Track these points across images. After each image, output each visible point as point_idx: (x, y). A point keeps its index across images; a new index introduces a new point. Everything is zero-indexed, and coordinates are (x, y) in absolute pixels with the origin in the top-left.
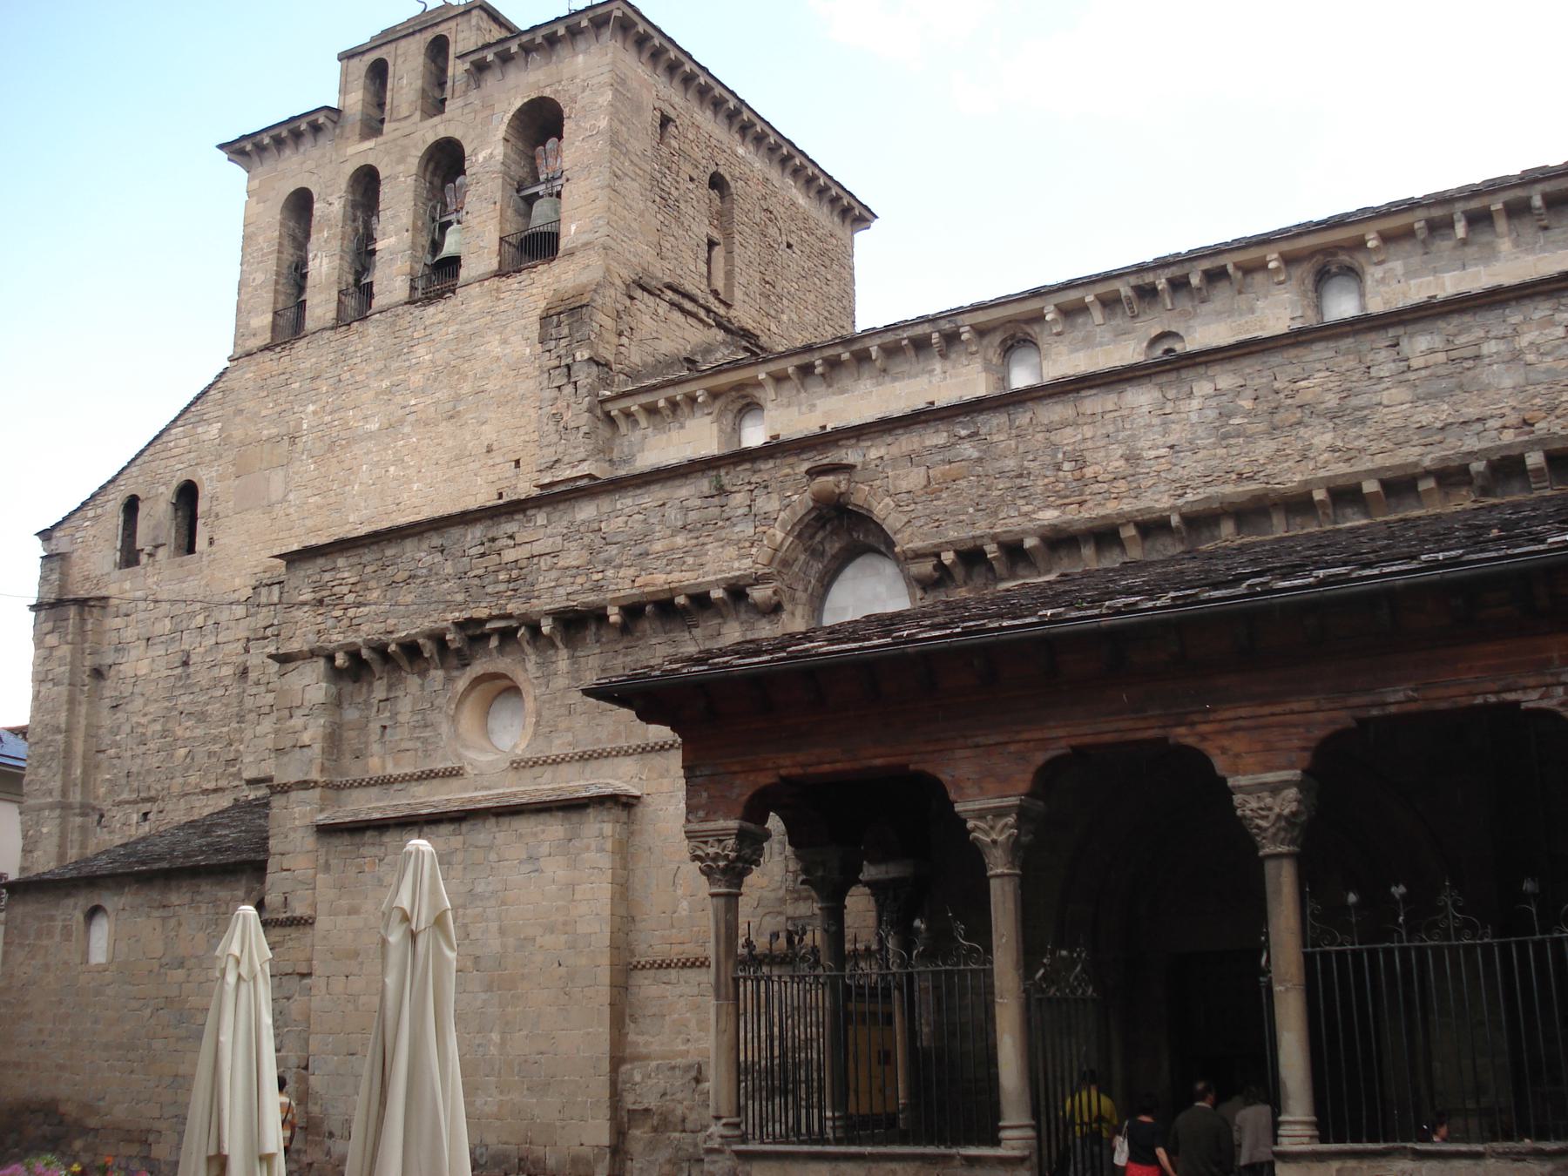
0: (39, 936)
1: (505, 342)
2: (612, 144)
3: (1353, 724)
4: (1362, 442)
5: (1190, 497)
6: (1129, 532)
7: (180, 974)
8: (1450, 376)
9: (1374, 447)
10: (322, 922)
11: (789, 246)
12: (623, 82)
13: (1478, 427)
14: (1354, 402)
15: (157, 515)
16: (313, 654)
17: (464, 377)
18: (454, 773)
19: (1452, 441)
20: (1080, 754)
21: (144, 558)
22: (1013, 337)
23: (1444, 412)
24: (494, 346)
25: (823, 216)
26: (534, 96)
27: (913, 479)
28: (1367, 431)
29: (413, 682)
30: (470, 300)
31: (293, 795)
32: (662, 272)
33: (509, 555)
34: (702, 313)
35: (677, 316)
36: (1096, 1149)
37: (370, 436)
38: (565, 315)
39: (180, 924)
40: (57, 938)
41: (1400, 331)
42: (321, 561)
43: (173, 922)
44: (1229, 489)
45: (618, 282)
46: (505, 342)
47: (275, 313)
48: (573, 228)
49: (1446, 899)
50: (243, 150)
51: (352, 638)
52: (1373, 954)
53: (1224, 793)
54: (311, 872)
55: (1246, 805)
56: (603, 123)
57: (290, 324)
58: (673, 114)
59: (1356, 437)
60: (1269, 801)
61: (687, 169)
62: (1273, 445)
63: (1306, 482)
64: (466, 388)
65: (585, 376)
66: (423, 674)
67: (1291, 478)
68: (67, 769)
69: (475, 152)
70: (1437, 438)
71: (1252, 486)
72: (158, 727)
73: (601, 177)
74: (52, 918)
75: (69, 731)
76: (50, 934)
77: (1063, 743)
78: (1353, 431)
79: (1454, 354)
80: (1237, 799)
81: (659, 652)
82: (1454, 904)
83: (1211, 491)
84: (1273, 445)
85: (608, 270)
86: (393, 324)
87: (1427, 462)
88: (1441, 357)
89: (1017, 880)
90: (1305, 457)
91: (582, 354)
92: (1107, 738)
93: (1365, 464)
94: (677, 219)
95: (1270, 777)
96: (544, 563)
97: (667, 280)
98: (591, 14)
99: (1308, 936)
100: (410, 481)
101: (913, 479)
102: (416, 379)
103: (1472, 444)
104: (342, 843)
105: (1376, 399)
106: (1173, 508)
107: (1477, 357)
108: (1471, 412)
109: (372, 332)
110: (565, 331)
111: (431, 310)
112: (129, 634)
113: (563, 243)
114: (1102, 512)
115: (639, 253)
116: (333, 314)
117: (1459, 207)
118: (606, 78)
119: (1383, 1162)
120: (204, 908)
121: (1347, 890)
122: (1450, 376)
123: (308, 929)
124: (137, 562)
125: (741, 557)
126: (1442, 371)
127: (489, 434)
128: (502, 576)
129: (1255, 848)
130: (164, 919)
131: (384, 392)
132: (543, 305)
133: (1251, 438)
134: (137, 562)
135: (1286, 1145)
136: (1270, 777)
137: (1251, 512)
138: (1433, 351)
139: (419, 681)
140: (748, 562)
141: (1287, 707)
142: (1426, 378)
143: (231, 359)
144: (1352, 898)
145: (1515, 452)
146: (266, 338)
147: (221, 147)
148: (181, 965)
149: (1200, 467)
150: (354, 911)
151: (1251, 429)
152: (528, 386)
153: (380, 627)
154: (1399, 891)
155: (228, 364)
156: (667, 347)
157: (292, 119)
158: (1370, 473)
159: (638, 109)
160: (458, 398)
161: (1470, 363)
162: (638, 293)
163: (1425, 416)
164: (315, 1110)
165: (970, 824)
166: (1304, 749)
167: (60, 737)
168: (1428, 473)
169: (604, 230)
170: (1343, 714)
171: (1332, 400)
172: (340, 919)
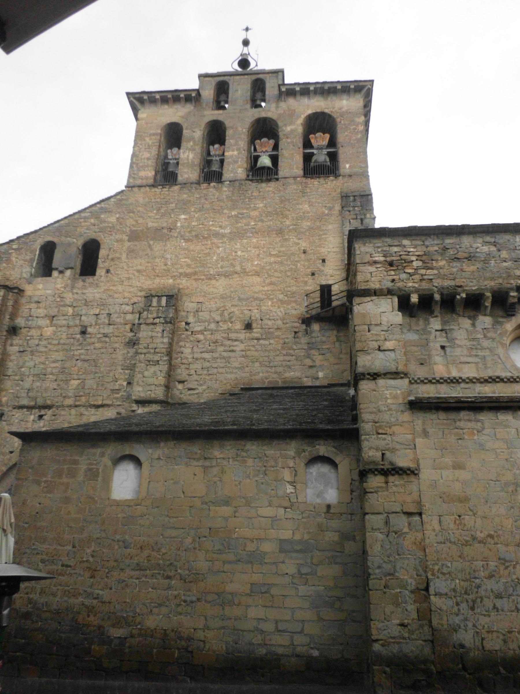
0: (59, 474)
7: (226, 511)
15: (68, 252)
16: (390, 292)
21: (55, 274)
26: (314, 111)
29: (466, 323)
31: (381, 382)
39: (223, 472)
40: (80, 478)
42: (389, 240)
43: (215, 471)
47: (156, 171)
48: (347, 166)
50: (139, 100)
51: (425, 285)
54: (410, 437)
57: (167, 175)
66: (473, 318)
74: (76, 462)
76: (72, 474)
98: (356, 84)
104: (434, 421)
120: (250, 462)
123: (412, 478)
124: (50, 275)
130: (205, 468)
134: (50, 275)
139: (469, 322)
143: (126, 187)
147: (128, 94)
148: (226, 502)
150: (458, 466)
155: (124, 188)
157: (176, 91)
172: (445, 473)
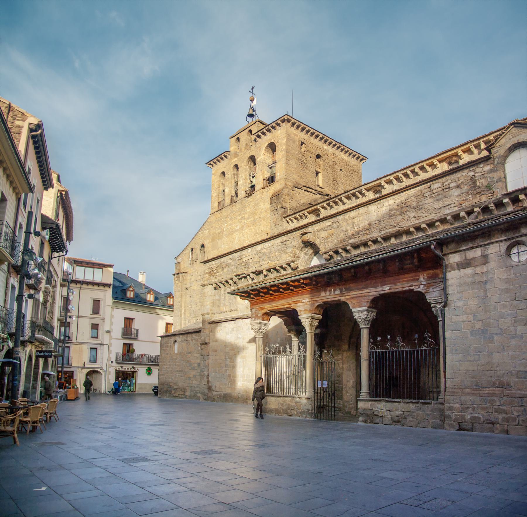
1: (264, 205)
2: (287, 152)
3: (378, 296)
4: (421, 215)
5: (382, 233)
6: (370, 243)
7: (190, 355)
8: (442, 194)
9: (425, 215)
10: (211, 344)
11: (341, 170)
12: (289, 135)
13: (449, 207)
14: (420, 204)
17: (256, 214)
18: (235, 310)
19: (442, 211)
20: (383, 297)
22: (376, 190)
23: (441, 204)
24: (262, 206)
25: (352, 161)
27: (323, 234)
28: (423, 211)
30: (257, 194)
32: (302, 182)
33: (244, 259)
34: (314, 191)
35: (306, 193)
36: (333, 397)
37: (237, 231)
38: (277, 196)
41: (431, 183)
44: (390, 230)
45: (289, 187)
46: (264, 205)
49: (398, 339)
52: (382, 352)
53: (352, 313)
55: (356, 316)
56: (284, 147)
58: (304, 141)
59: (420, 213)
60: (361, 315)
61: (310, 155)
62: (401, 217)
63: (408, 226)
64: (257, 217)
65: (281, 211)
67: (405, 225)
68: (181, 310)
69: (258, 158)
70: (439, 211)
71: (396, 229)
72: (199, 301)
73: (284, 160)
75: (181, 302)
77: (320, 301)
78: (419, 212)
79: (443, 188)
80: (354, 314)
81: (244, 284)
82: (428, 336)
83: (387, 231)
84: (401, 217)
85: (286, 184)
86: (241, 203)
87: (436, 218)
88: (440, 189)
89: (368, 330)
90: (408, 220)
91: (279, 206)
92: (329, 300)
93: (422, 220)
94: (306, 168)
95: (361, 309)
96: (251, 261)
97: (304, 184)
99: (370, 348)
100: (245, 241)
101: (323, 234)
102: (246, 216)
103: (447, 212)
105: (425, 202)
106: (378, 236)
107: (449, 188)
108: (447, 203)
109: (238, 205)
110: (276, 201)
111: (249, 198)
112: (193, 280)
113: (277, 179)
114: (363, 239)
115: (296, 178)
116: (230, 202)
117: (481, 141)
118: (285, 135)
119: (380, 403)
121: (377, 338)
122: (442, 194)
125: (289, 256)
126: (440, 193)
127: (261, 227)
128: (243, 264)
129: (359, 326)
131: (240, 220)
132: (271, 195)
133: (396, 216)
135: (361, 398)
136: (361, 309)
137: (398, 235)
138: (438, 188)
140: (290, 258)
141: (364, 292)
142: (437, 195)
144: (389, 337)
145: (457, 213)
146: (217, 209)
149: (385, 225)
151: (396, 214)
152: (269, 215)
153: (221, 278)
154: (379, 339)
156: (302, 201)
158: (423, 222)
159: (294, 142)
160: (255, 220)
161: (447, 190)
162: (295, 189)
163: (436, 206)
164: (210, 385)
165: (432, 305)
166: (368, 302)
167: (180, 304)
168: (437, 221)
169: (285, 174)
170: (376, 293)
171: (414, 204)
